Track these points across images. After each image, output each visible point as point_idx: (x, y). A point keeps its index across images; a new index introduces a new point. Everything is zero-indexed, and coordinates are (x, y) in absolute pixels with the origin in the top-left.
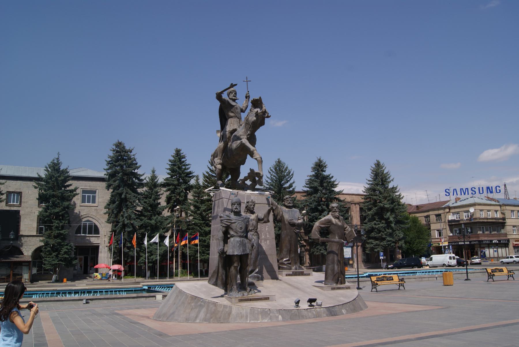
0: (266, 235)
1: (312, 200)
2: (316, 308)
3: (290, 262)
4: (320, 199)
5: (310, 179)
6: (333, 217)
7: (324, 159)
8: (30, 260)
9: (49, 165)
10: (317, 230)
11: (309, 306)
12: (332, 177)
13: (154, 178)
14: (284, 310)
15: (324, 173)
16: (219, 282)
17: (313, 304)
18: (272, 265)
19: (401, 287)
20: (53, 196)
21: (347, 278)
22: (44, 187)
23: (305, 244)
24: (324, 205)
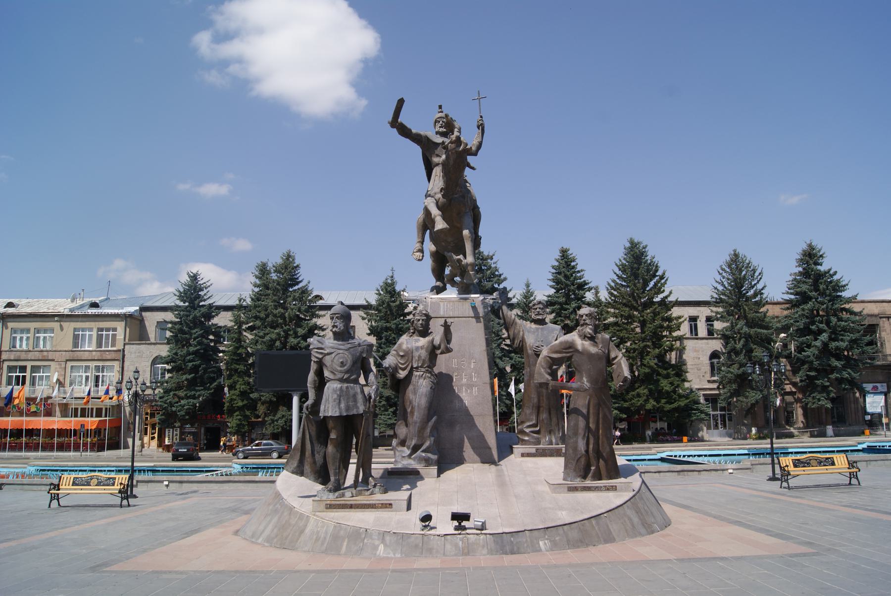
0: (471, 378)
1: (799, 315)
2: (468, 534)
3: (538, 429)
4: (815, 312)
5: (795, 279)
7: (818, 243)
8: (321, 415)
9: (381, 287)
10: (543, 364)
11: (456, 528)
12: (835, 273)
13: (528, 295)
14: (394, 533)
15: (819, 267)
16: (307, 468)
17: (464, 523)
18: (483, 436)
19: (853, 479)
20: (387, 329)
22: (375, 317)
23: (794, 390)
24: (821, 322)
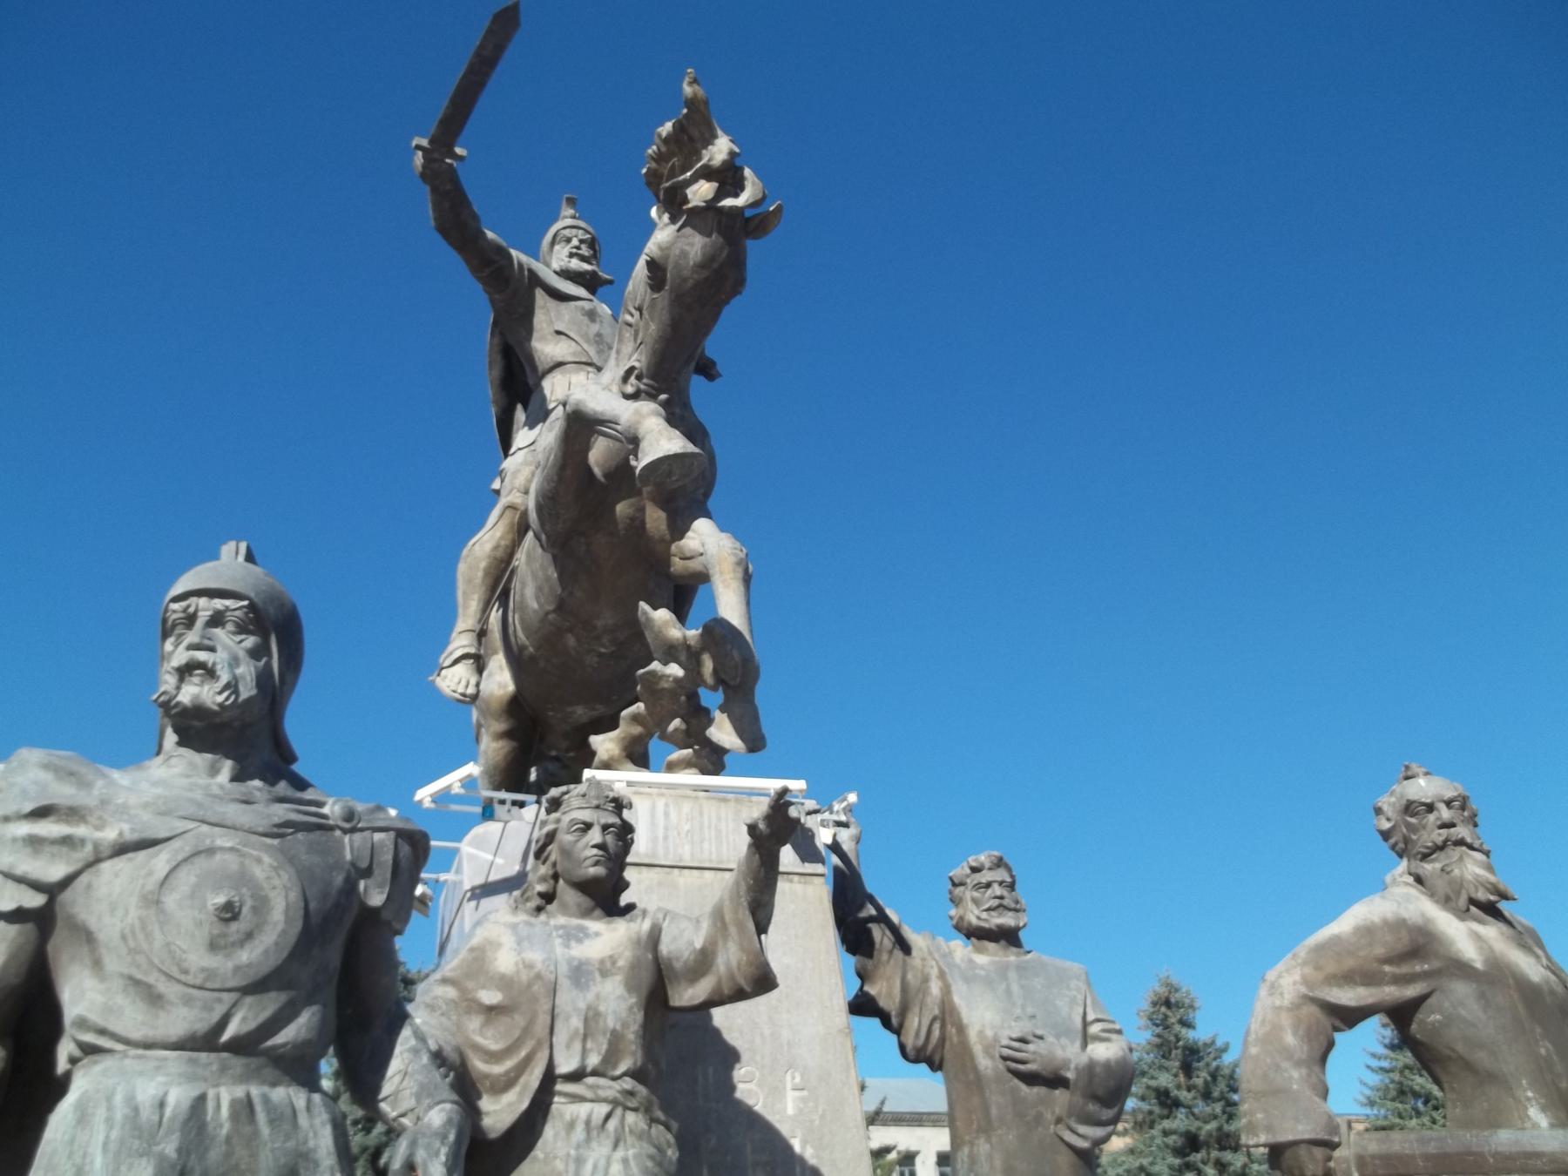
6: (1446, 902)
10: (1290, 1039)
15: (1190, 1035)
21: (561, 1094)
